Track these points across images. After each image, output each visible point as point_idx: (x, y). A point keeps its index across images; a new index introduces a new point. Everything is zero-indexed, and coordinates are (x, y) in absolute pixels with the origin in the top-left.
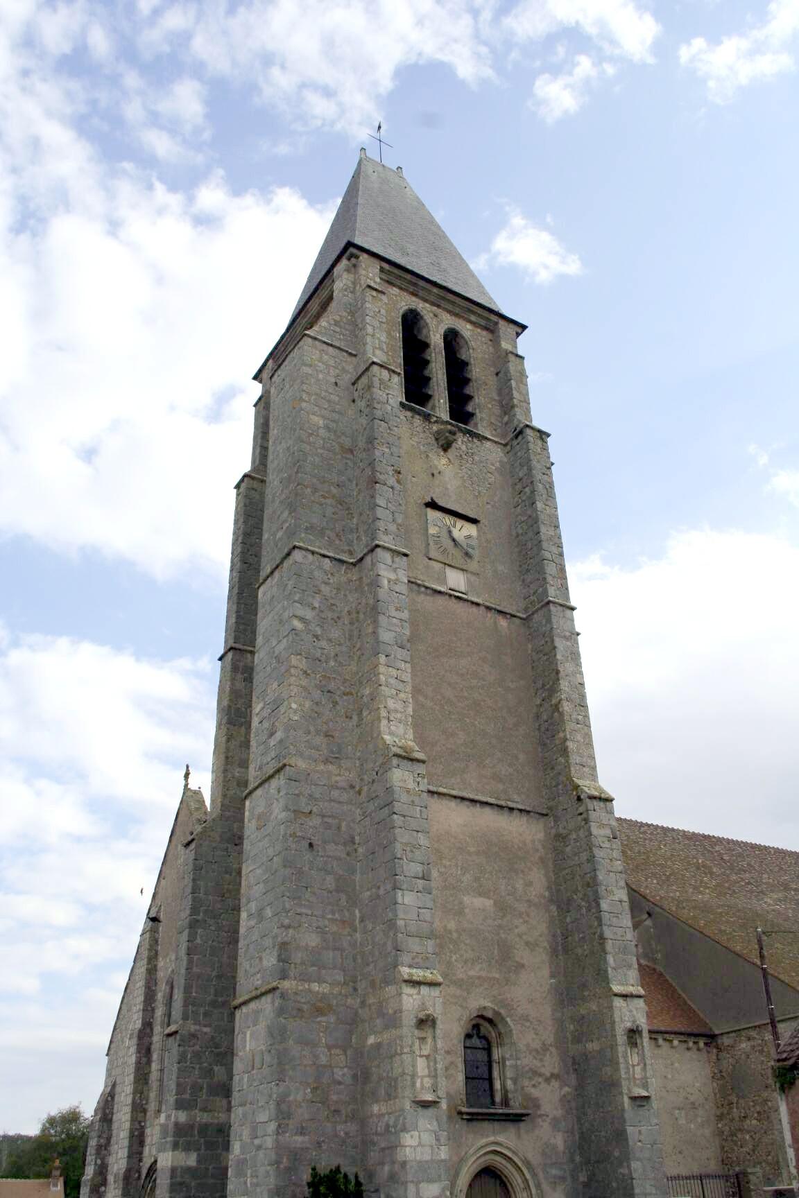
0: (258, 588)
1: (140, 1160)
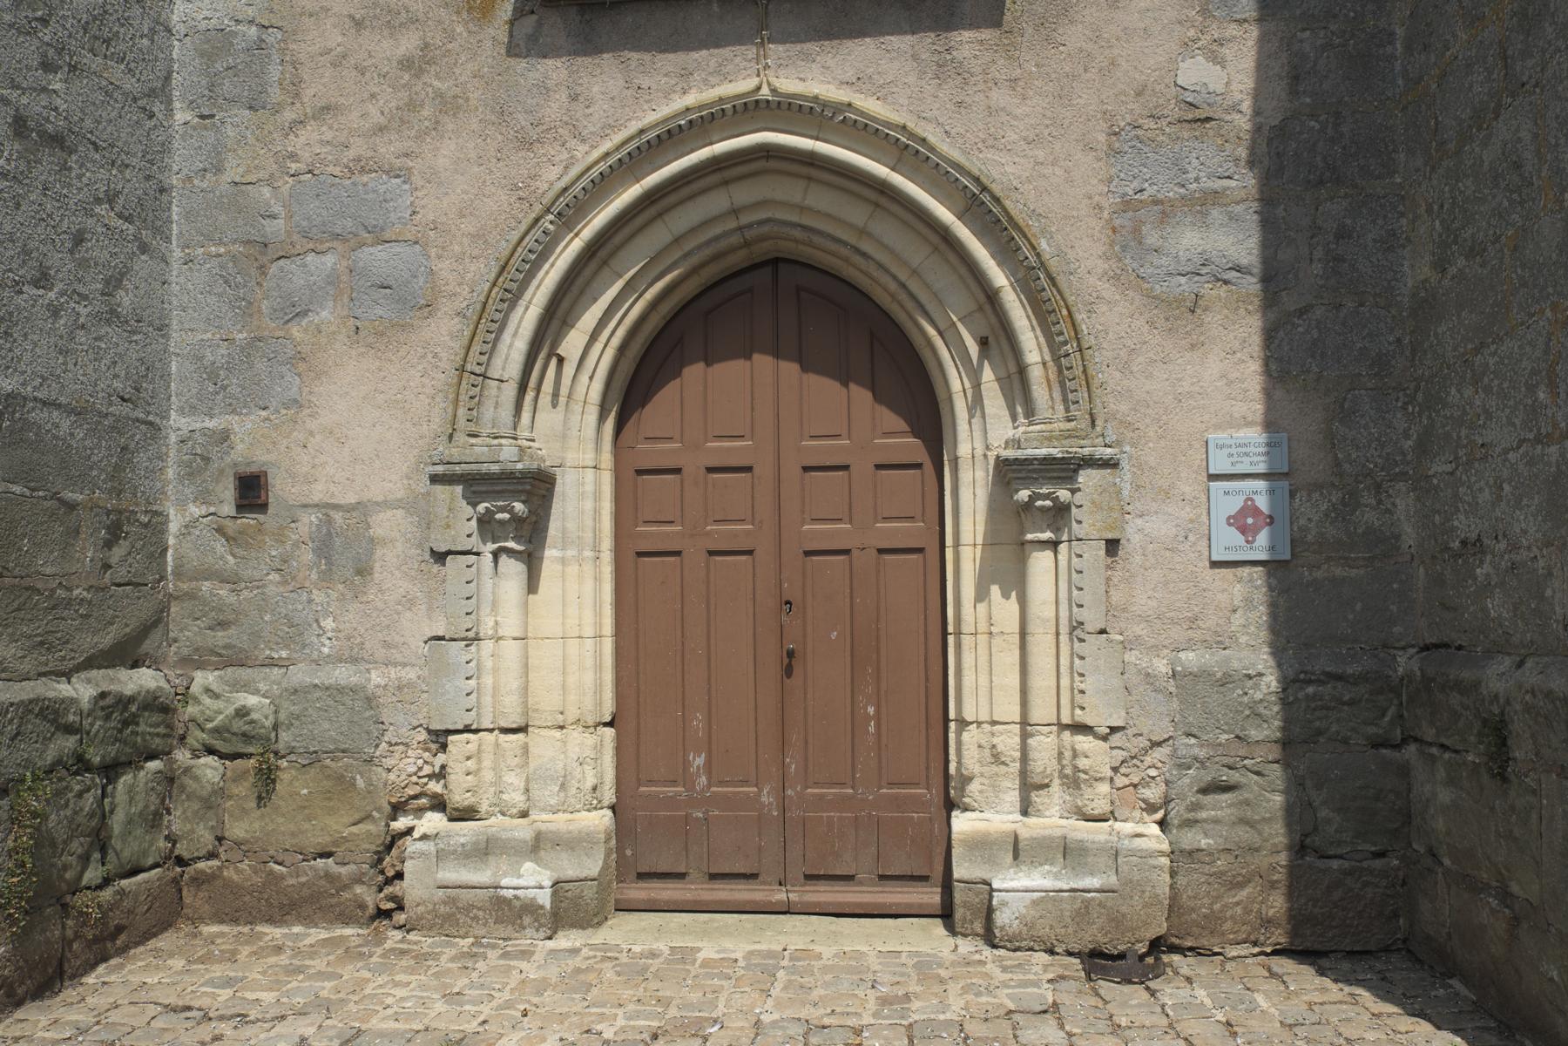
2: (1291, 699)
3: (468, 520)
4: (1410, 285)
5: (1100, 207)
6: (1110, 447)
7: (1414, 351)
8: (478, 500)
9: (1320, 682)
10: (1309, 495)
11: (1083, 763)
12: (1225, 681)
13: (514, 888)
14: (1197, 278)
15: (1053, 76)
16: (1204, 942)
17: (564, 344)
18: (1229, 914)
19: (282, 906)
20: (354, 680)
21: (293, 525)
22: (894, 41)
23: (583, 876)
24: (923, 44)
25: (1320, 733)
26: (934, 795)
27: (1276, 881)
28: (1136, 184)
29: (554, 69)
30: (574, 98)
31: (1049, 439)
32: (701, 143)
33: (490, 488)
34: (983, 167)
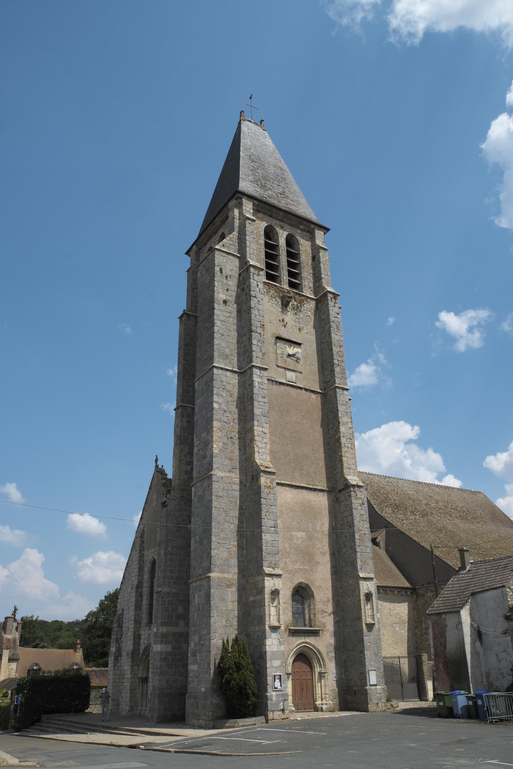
0: (195, 382)
1: (139, 646)
26: (313, 701)
29: (291, 638)
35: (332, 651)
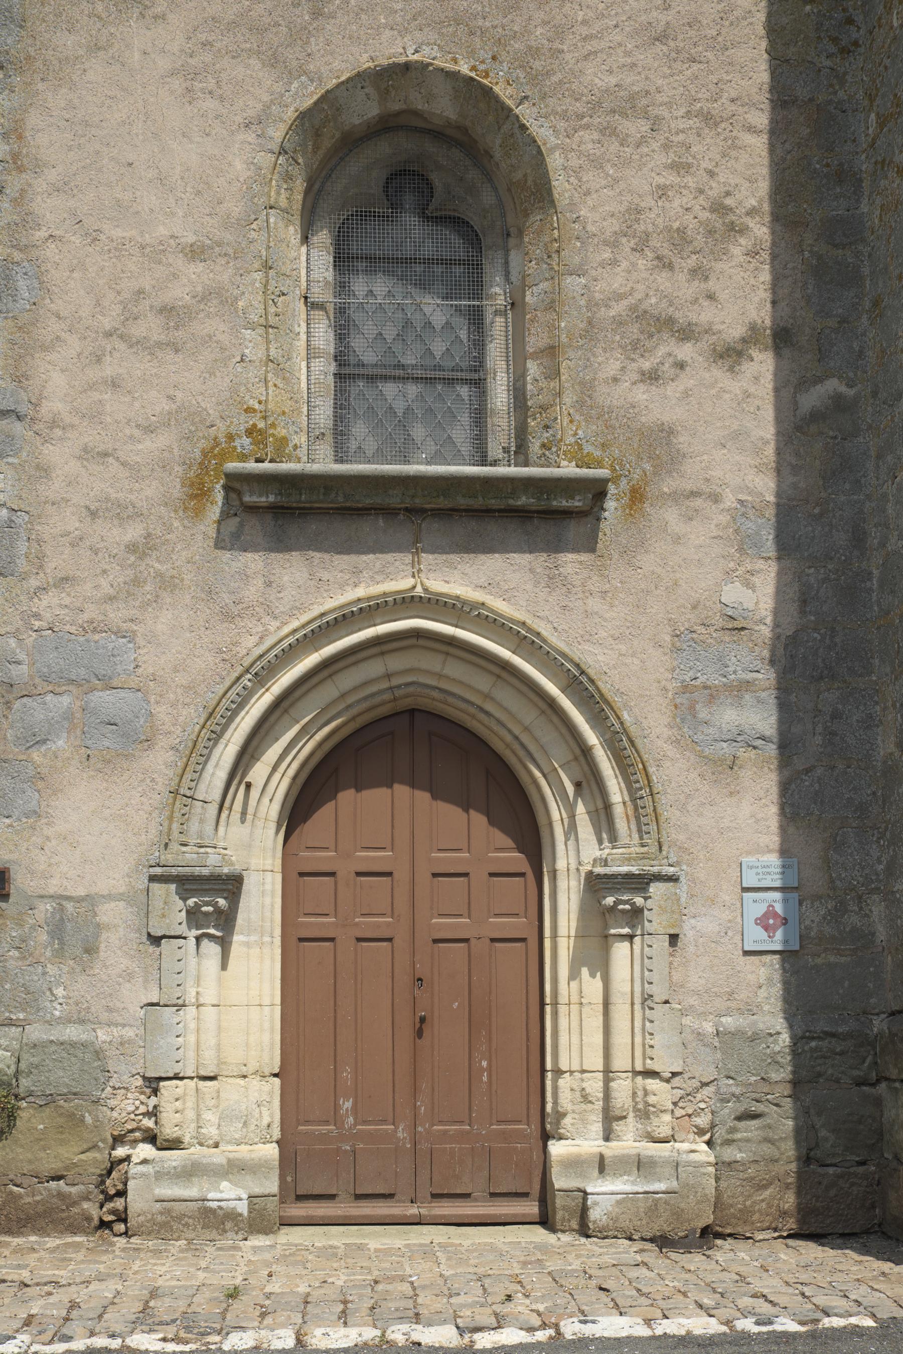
2: (800, 1050)
3: (180, 911)
4: (882, 754)
5: (665, 689)
6: (672, 866)
7: (884, 801)
8: (188, 896)
9: (819, 1038)
10: (812, 903)
11: (651, 1099)
12: (754, 1038)
13: (218, 1201)
14: (735, 744)
15: (633, 591)
16: (739, 1230)
17: (251, 773)
18: (757, 1208)
19: (19, 1220)
20: (84, 1037)
21: (30, 912)
22: (516, 557)
23: (267, 1192)
24: (539, 561)
25: (820, 1075)
26: (534, 1129)
27: (790, 1183)
28: (691, 674)
29: (253, 561)
30: (269, 584)
31: (629, 859)
32: (366, 624)
33: (199, 887)
34: (581, 656)
35: (746, 685)
